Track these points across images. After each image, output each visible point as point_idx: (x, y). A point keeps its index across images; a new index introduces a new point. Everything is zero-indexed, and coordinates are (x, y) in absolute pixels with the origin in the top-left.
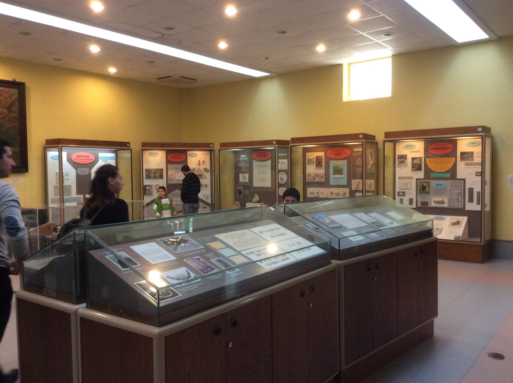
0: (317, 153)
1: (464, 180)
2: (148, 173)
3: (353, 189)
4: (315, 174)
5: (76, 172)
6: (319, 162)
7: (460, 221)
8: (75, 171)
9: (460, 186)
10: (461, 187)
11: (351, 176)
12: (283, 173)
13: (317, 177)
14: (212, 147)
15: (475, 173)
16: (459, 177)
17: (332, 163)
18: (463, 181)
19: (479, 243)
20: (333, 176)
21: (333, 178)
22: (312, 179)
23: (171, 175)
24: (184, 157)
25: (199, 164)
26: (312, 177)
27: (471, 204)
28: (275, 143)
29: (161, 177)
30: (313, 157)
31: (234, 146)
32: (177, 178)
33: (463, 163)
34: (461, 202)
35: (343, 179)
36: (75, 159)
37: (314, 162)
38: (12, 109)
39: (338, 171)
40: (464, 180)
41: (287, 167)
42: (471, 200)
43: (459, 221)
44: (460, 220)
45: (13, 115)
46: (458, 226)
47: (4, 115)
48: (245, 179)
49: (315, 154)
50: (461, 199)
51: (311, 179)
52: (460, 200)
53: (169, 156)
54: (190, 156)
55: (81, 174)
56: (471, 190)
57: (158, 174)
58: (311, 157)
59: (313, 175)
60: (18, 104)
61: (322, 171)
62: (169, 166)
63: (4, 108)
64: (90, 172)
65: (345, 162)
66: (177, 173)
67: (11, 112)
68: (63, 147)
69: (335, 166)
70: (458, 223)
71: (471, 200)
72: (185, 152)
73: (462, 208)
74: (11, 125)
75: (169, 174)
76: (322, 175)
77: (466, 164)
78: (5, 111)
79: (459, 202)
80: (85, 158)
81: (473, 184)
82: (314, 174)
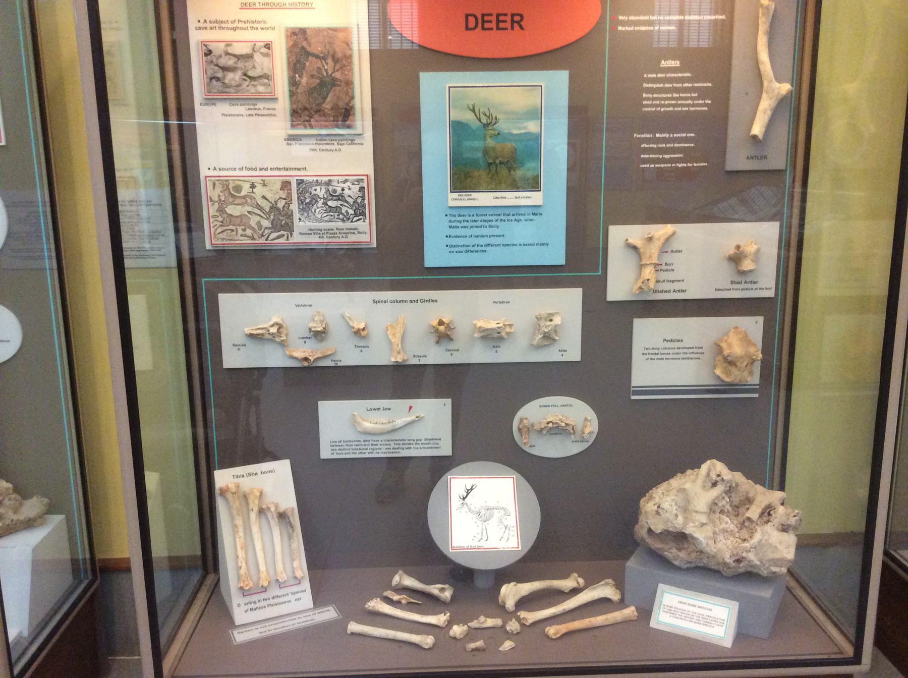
13: (306, 206)
22: (266, 223)
26: (266, 206)
59: (273, 192)
76: (352, 191)
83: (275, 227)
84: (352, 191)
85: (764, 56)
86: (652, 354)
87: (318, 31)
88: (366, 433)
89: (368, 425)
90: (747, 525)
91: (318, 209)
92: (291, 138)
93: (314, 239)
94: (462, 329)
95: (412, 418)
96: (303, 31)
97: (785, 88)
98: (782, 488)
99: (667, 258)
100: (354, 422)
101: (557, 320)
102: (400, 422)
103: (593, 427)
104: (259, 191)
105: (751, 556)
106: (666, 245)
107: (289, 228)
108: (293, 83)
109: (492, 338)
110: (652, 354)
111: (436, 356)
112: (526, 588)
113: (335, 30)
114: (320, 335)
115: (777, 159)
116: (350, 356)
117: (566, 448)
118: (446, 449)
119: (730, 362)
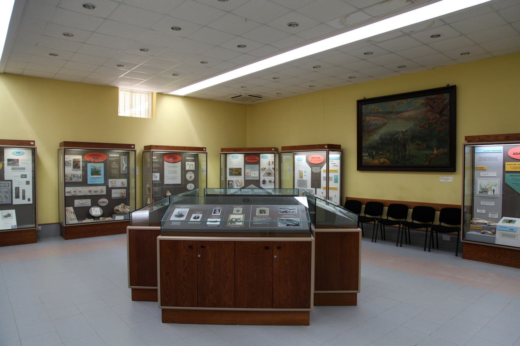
0: (74, 156)
1: (11, 181)
2: (231, 171)
3: (110, 186)
4: (72, 175)
5: (312, 170)
6: (76, 165)
7: (10, 214)
8: (311, 169)
9: (8, 186)
10: (9, 186)
11: (107, 177)
12: (192, 172)
13: (74, 177)
14: (204, 151)
15: (20, 176)
16: (6, 178)
17: (90, 166)
18: (10, 182)
19: (35, 227)
20: (91, 176)
21: (91, 179)
22: (69, 179)
23: (248, 173)
24: (258, 158)
25: (269, 164)
26: (69, 177)
27: (18, 199)
28: (326, 147)
29: (240, 174)
30: (70, 159)
31: (167, 148)
32: (252, 175)
33: (10, 167)
34: (8, 198)
35: (100, 179)
36: (311, 160)
37: (70, 164)
38: (444, 113)
39: (95, 172)
40: (11, 181)
41: (194, 168)
42: (17, 197)
43: (9, 214)
44: (10, 213)
45: (444, 118)
46: (10, 217)
47: (436, 120)
48: (156, 177)
49: (72, 156)
50: (8, 195)
51: (68, 179)
52: (8, 197)
53: (246, 158)
54: (263, 157)
55: (315, 172)
56: (17, 189)
57: (237, 172)
58: (68, 159)
59: (70, 176)
60: (449, 107)
61: (79, 172)
62: (246, 165)
63: (437, 113)
64: (321, 170)
65: (103, 164)
66: (251, 172)
67: (443, 116)
68: (66, 149)
69: (92, 168)
70: (9, 215)
71: (17, 197)
72: (258, 155)
73: (10, 203)
74: (442, 127)
75: (246, 172)
76: (79, 176)
77: (13, 169)
78: (438, 116)
79: (7, 198)
80: (318, 159)
81: (19, 184)
82: (71, 175)
83: (70, 179)
84: (79, 176)
85: (124, 162)
86: (114, 193)
87: (76, 159)
88: (80, 203)
89: (81, 202)
90: (124, 208)
91: (75, 178)
92: (73, 170)
93: (75, 181)
94: (92, 191)
95: (86, 201)
96: (75, 159)
97: (126, 165)
98: (129, 206)
99: (115, 183)
100: (79, 202)
101: (103, 189)
102: (85, 202)
103: (108, 202)
104: (69, 175)
105: (124, 211)
106: (115, 180)
107: (72, 180)
108: (73, 164)
109: (96, 192)
110: (114, 193)
111: (89, 194)
112: (103, 218)
113: (78, 159)
114: (75, 192)
115: (126, 172)
116: (79, 194)
117: (104, 205)
118: (90, 205)
119: (122, 193)
